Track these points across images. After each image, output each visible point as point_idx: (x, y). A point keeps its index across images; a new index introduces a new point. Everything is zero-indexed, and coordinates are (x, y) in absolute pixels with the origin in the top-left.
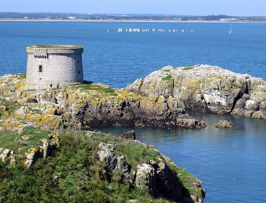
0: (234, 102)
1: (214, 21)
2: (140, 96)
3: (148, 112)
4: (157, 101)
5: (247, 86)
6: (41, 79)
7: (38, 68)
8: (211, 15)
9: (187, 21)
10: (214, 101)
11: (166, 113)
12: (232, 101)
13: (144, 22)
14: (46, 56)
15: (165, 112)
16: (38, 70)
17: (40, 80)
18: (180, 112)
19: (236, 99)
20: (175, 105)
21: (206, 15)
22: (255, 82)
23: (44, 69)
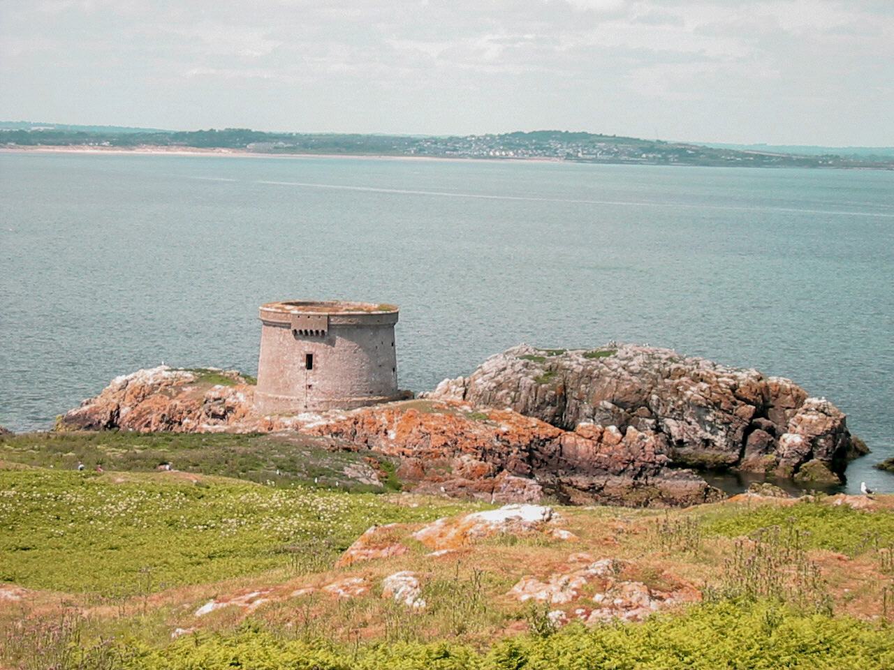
0: (743, 437)
1: (223, 150)
2: (557, 430)
3: (585, 464)
4: (600, 440)
5: (763, 398)
6: (310, 386)
7: (301, 361)
8: (206, 129)
9: (78, 148)
10: (692, 436)
11: (631, 467)
12: (739, 435)
13: (97, 154)
14: (326, 331)
15: (628, 464)
16: (304, 364)
17: (309, 391)
18: (662, 465)
19: (748, 431)
20: (646, 449)
21: (499, 130)
22: (779, 390)
23: (318, 361)
